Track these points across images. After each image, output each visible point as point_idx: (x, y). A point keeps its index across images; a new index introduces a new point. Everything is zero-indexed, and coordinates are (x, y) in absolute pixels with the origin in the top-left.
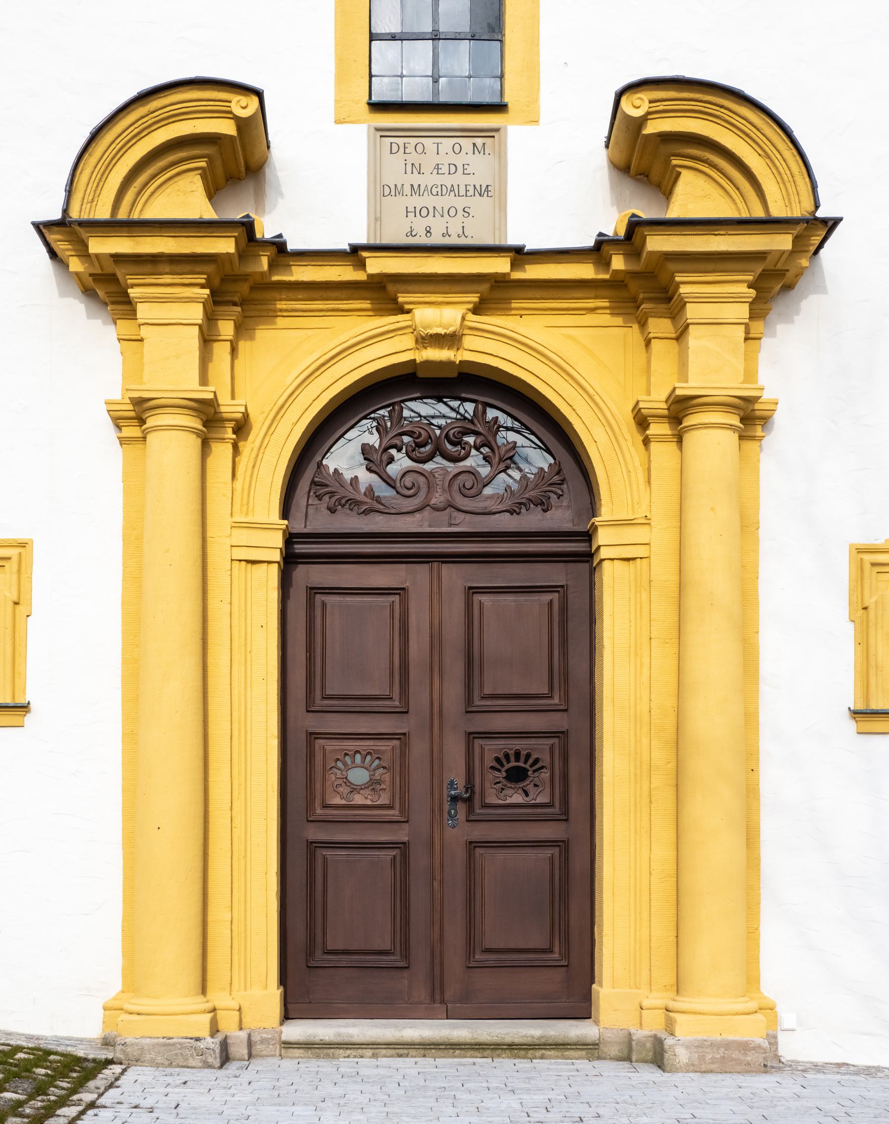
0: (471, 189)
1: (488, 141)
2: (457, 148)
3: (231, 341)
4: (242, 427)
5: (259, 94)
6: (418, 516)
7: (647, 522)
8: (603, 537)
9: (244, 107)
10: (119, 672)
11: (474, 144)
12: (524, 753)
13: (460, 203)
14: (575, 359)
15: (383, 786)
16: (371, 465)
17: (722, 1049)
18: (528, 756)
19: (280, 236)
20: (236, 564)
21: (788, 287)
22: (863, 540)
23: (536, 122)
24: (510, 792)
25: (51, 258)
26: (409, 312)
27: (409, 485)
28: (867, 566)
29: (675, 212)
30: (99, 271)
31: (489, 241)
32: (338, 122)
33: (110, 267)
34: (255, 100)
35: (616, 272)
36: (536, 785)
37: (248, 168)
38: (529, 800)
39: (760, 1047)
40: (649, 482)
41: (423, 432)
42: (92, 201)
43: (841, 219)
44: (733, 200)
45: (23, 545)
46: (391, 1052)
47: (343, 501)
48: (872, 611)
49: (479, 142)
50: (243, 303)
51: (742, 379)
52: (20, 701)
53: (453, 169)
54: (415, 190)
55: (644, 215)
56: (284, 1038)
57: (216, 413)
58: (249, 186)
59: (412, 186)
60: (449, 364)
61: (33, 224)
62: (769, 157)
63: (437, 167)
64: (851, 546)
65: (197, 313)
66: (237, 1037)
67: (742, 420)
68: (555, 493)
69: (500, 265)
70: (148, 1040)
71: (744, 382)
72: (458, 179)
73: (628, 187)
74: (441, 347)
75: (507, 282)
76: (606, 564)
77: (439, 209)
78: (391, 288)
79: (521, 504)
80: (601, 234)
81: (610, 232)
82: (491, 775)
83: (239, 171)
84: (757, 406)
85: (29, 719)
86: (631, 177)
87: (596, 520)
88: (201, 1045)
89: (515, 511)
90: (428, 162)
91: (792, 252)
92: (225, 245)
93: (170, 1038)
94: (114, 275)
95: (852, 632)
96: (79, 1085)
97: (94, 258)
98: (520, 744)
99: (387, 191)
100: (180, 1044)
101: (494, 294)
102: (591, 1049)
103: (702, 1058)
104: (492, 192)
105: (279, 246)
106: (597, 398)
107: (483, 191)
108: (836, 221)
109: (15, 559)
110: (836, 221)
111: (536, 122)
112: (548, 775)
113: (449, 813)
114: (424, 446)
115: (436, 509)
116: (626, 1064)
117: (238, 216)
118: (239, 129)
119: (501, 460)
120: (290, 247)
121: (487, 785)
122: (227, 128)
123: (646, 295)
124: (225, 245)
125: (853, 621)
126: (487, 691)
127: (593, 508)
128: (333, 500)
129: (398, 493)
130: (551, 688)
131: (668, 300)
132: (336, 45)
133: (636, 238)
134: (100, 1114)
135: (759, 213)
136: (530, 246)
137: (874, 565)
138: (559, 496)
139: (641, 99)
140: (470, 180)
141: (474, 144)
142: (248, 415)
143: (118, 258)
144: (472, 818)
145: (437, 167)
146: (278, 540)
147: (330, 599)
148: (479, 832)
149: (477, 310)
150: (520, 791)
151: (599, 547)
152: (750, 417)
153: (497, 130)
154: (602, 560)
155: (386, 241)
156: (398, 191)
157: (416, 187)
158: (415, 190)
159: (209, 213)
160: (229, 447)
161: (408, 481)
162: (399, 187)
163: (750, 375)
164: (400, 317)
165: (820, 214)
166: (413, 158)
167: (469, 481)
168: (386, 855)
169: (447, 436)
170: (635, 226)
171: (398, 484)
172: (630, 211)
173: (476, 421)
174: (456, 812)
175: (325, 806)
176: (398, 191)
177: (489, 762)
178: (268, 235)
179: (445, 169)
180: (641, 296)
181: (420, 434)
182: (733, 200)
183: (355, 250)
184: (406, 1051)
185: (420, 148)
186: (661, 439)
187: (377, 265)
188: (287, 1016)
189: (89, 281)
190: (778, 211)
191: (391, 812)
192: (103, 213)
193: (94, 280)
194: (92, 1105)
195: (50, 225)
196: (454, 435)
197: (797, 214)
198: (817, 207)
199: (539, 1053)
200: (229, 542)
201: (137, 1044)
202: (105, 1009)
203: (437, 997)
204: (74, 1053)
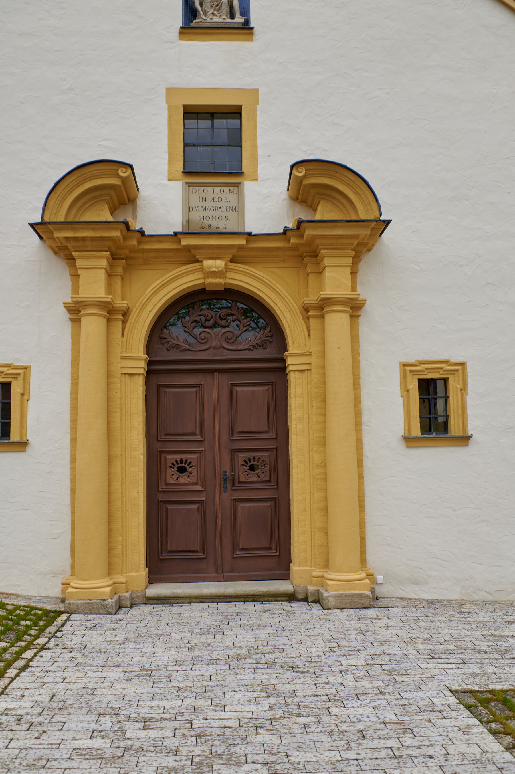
0: (228, 208)
1: (236, 188)
2: (222, 191)
4: (126, 314)
5: (131, 167)
8: (290, 361)
9: (123, 173)
10: (69, 425)
13: (223, 214)
14: (272, 286)
15: (193, 474)
16: (186, 329)
17: (350, 598)
19: (142, 228)
21: (369, 250)
22: (468, 365)
23: (257, 180)
24: (251, 476)
25: (40, 239)
26: (201, 262)
27: (203, 338)
28: (408, 372)
29: (318, 217)
31: (236, 230)
32: (169, 180)
33: (65, 244)
34: (129, 171)
36: (263, 473)
37: (129, 200)
39: (367, 596)
40: (309, 336)
41: (209, 315)
42: (56, 213)
43: (391, 221)
44: (339, 207)
45: (26, 368)
46: (198, 600)
47: (173, 345)
48: (411, 392)
49: (232, 188)
50: (126, 258)
51: (350, 290)
52: (24, 440)
53: (220, 200)
54: (204, 209)
55: (304, 219)
56: (147, 595)
57: (113, 307)
58: (130, 208)
60: (220, 284)
62: (358, 193)
63: (213, 199)
64: (400, 363)
65: (104, 263)
66: (125, 596)
68: (269, 341)
69: (242, 241)
70: (80, 601)
71: (352, 291)
72: (223, 204)
73: (298, 208)
75: (249, 248)
76: (292, 373)
77: (214, 217)
78: (193, 252)
79: (253, 346)
80: (285, 227)
81: (290, 226)
82: (170, 471)
83: (125, 201)
85: (28, 449)
86: (299, 203)
88: (106, 603)
90: (210, 196)
92: (116, 234)
94: (67, 246)
95: (402, 401)
96: (49, 624)
97: (57, 239)
98: (184, 457)
99: (191, 209)
100: (95, 603)
102: (291, 597)
103: (341, 602)
104: (238, 209)
105: (142, 233)
106: (286, 298)
108: (389, 222)
109: (22, 375)
110: (389, 222)
111: (257, 180)
113: (223, 486)
114: (209, 320)
117: (122, 220)
118: (123, 182)
120: (146, 234)
121: (241, 472)
123: (307, 254)
124: (116, 234)
125: (403, 397)
126: (240, 430)
128: (169, 345)
130: (269, 428)
131: (315, 255)
132: (168, 148)
134: (44, 655)
135: (354, 218)
137: (411, 371)
138: (271, 342)
139: (302, 169)
140: (228, 205)
143: (67, 238)
144: (234, 488)
145: (213, 199)
146: (143, 364)
147: (168, 390)
148: (237, 496)
150: (256, 475)
151: (289, 365)
152: (355, 308)
153: (240, 183)
155: (190, 231)
156: (196, 209)
157: (204, 208)
158: (204, 209)
159: (110, 219)
160: (120, 323)
161: (202, 336)
162: (196, 207)
163: (354, 288)
164: (197, 264)
166: (203, 195)
167: (230, 335)
168: (195, 507)
170: (300, 223)
171: (198, 338)
174: (227, 486)
175: (167, 484)
176: (196, 209)
177: (241, 462)
179: (217, 200)
180: (304, 254)
181: (208, 316)
182: (339, 207)
183: (176, 234)
184: (204, 600)
185: (205, 191)
186: (315, 317)
187: (185, 241)
188: (152, 580)
192: (62, 220)
193: (58, 249)
194: (43, 648)
197: (372, 218)
198: (381, 215)
200: (120, 365)
201: (75, 603)
202: (63, 584)
203: (220, 571)
204: (46, 608)
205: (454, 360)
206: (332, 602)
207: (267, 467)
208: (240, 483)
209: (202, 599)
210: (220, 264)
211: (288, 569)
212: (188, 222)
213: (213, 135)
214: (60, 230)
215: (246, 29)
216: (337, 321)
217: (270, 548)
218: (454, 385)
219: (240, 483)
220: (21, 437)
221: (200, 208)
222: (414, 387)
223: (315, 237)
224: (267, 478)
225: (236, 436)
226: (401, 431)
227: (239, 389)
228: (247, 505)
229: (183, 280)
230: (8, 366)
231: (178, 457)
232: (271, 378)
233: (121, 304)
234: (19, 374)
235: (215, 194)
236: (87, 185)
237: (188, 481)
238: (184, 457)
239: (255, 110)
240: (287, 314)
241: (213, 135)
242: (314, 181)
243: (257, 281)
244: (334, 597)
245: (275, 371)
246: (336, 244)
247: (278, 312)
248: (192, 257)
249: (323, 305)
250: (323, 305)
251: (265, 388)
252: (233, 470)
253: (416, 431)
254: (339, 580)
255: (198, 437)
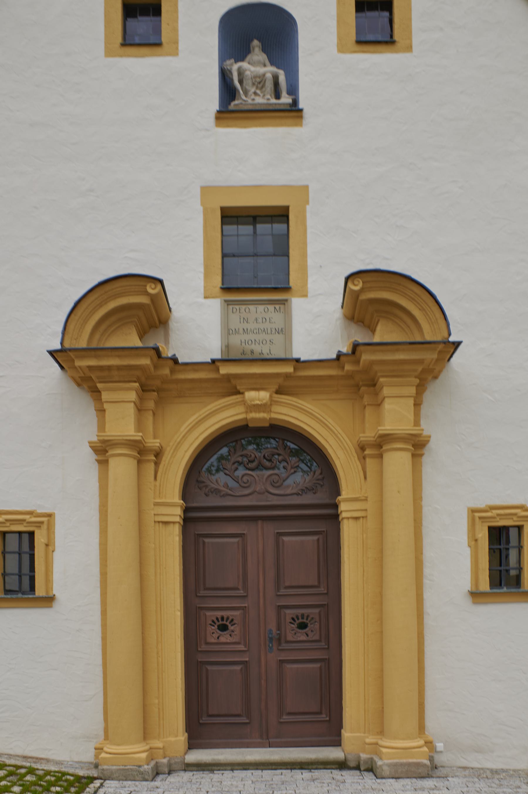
0: (274, 331)
2: (266, 310)
3: (152, 410)
4: (158, 454)
5: (161, 282)
6: (251, 497)
7: (366, 500)
9: (152, 289)
11: (275, 308)
12: (306, 615)
13: (268, 337)
18: (308, 616)
20: (157, 524)
21: (436, 377)
27: (245, 481)
28: (477, 519)
29: (377, 339)
30: (83, 375)
31: (283, 356)
32: (206, 297)
34: (159, 287)
35: (348, 371)
37: (160, 322)
38: (309, 638)
47: (212, 490)
48: (479, 542)
49: (277, 307)
51: (413, 424)
52: (51, 595)
55: (360, 341)
56: (186, 761)
57: (144, 446)
59: (244, 329)
60: (264, 419)
61: (48, 351)
62: (424, 310)
64: (468, 509)
65: (133, 396)
67: (413, 446)
69: (289, 369)
72: (267, 325)
74: (260, 412)
75: (297, 377)
76: (345, 521)
84: (421, 439)
85: (55, 604)
87: (339, 498)
88: (142, 769)
89: (299, 494)
91: (437, 360)
92: (145, 361)
93: (125, 766)
94: (91, 377)
98: (225, 614)
99: (231, 331)
100: (131, 769)
101: (284, 388)
102: (342, 765)
104: (286, 331)
106: (339, 435)
107: (279, 331)
109: (46, 523)
112: (318, 626)
115: (259, 493)
116: (357, 772)
117: (151, 345)
118: (152, 301)
119: (292, 468)
122: (143, 300)
124: (145, 361)
126: (287, 584)
127: (338, 493)
128: (207, 490)
129: (240, 485)
130: (319, 582)
131: (373, 384)
133: (357, 353)
136: (302, 359)
138: (322, 486)
141: (275, 308)
142: (162, 447)
143: (90, 368)
146: (178, 511)
147: (207, 540)
148: (283, 656)
149: (278, 392)
150: (305, 634)
151: (341, 512)
152: (418, 445)
154: (343, 519)
155: (231, 357)
156: (237, 332)
157: (245, 330)
159: (139, 344)
160: (153, 465)
161: (245, 479)
162: (237, 330)
163: (417, 423)
165: (451, 339)
167: (276, 478)
168: (238, 668)
169: (264, 456)
170: (355, 346)
171: (240, 481)
172: (353, 340)
173: (279, 448)
175: (207, 643)
176: (237, 332)
177: (288, 620)
178: (170, 355)
179: (260, 320)
183: (214, 361)
185: (247, 310)
186: (372, 456)
187: (224, 370)
189: (79, 380)
190: (428, 338)
191: (240, 646)
192: (83, 344)
195: (57, 351)
196: (268, 456)
198: (450, 334)
199: (314, 767)
202: (96, 749)
205: (39, 511)
206: (386, 771)
207: (317, 626)
208: (287, 642)
209: (245, 766)
210: (263, 396)
211: (339, 735)
212: (227, 347)
213: (255, 241)
214: (82, 357)
215: (293, 112)
216: (397, 461)
217: (320, 713)
218: (40, 540)
219: (287, 642)
220: (47, 592)
221: (241, 331)
222: (483, 535)
223: (372, 363)
224: (317, 637)
225: (283, 591)
226: (467, 585)
227: (286, 539)
228: (295, 666)
229: (224, 414)
230: (31, 513)
231: (219, 614)
232: (321, 526)
233: (153, 443)
234: (42, 523)
235: (258, 314)
236: (112, 305)
237: (229, 640)
238: (225, 614)
239: (304, 211)
240: (340, 453)
241: (255, 241)
242: (372, 295)
243: (302, 414)
244: (389, 765)
245: (329, 517)
246: (398, 371)
247: (330, 451)
248: (231, 388)
249: (382, 443)
250: (382, 443)
251: (315, 538)
252: (279, 628)
253: (485, 586)
254: (394, 748)
255: (241, 592)
